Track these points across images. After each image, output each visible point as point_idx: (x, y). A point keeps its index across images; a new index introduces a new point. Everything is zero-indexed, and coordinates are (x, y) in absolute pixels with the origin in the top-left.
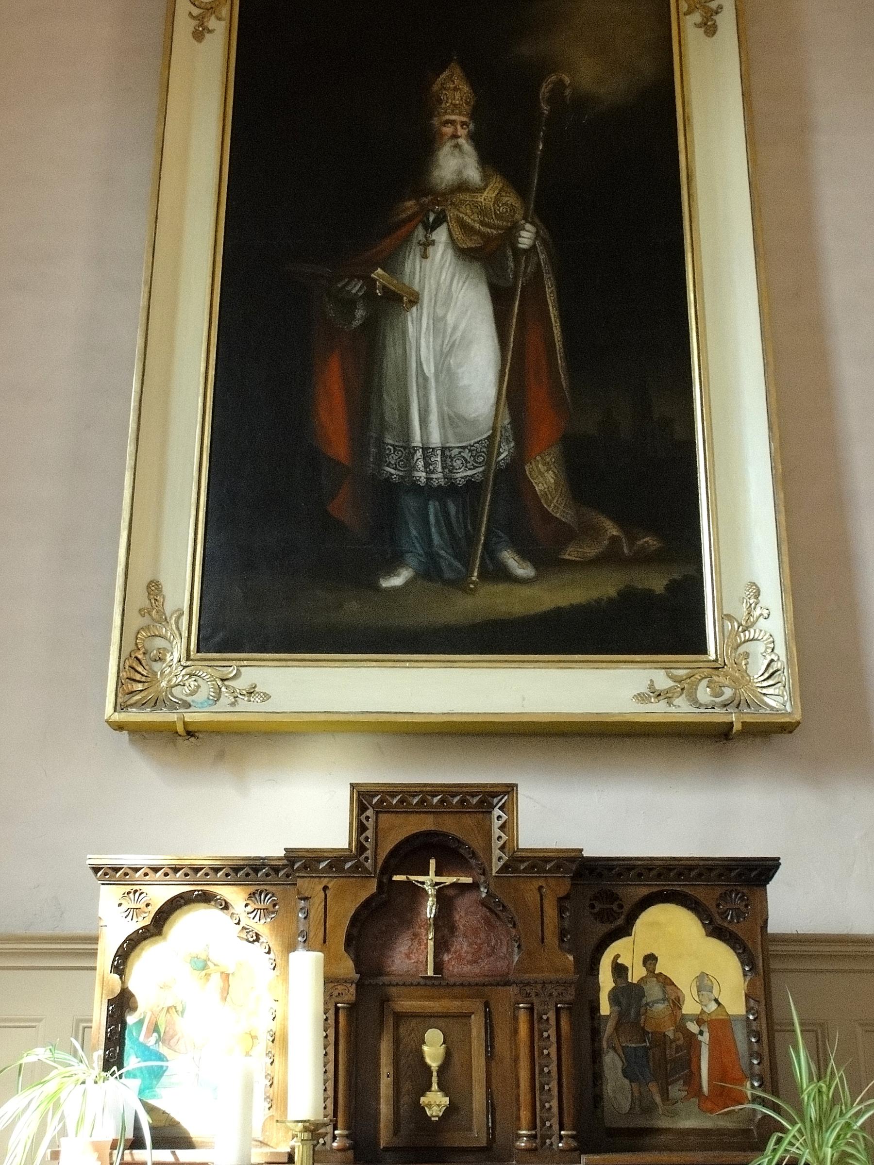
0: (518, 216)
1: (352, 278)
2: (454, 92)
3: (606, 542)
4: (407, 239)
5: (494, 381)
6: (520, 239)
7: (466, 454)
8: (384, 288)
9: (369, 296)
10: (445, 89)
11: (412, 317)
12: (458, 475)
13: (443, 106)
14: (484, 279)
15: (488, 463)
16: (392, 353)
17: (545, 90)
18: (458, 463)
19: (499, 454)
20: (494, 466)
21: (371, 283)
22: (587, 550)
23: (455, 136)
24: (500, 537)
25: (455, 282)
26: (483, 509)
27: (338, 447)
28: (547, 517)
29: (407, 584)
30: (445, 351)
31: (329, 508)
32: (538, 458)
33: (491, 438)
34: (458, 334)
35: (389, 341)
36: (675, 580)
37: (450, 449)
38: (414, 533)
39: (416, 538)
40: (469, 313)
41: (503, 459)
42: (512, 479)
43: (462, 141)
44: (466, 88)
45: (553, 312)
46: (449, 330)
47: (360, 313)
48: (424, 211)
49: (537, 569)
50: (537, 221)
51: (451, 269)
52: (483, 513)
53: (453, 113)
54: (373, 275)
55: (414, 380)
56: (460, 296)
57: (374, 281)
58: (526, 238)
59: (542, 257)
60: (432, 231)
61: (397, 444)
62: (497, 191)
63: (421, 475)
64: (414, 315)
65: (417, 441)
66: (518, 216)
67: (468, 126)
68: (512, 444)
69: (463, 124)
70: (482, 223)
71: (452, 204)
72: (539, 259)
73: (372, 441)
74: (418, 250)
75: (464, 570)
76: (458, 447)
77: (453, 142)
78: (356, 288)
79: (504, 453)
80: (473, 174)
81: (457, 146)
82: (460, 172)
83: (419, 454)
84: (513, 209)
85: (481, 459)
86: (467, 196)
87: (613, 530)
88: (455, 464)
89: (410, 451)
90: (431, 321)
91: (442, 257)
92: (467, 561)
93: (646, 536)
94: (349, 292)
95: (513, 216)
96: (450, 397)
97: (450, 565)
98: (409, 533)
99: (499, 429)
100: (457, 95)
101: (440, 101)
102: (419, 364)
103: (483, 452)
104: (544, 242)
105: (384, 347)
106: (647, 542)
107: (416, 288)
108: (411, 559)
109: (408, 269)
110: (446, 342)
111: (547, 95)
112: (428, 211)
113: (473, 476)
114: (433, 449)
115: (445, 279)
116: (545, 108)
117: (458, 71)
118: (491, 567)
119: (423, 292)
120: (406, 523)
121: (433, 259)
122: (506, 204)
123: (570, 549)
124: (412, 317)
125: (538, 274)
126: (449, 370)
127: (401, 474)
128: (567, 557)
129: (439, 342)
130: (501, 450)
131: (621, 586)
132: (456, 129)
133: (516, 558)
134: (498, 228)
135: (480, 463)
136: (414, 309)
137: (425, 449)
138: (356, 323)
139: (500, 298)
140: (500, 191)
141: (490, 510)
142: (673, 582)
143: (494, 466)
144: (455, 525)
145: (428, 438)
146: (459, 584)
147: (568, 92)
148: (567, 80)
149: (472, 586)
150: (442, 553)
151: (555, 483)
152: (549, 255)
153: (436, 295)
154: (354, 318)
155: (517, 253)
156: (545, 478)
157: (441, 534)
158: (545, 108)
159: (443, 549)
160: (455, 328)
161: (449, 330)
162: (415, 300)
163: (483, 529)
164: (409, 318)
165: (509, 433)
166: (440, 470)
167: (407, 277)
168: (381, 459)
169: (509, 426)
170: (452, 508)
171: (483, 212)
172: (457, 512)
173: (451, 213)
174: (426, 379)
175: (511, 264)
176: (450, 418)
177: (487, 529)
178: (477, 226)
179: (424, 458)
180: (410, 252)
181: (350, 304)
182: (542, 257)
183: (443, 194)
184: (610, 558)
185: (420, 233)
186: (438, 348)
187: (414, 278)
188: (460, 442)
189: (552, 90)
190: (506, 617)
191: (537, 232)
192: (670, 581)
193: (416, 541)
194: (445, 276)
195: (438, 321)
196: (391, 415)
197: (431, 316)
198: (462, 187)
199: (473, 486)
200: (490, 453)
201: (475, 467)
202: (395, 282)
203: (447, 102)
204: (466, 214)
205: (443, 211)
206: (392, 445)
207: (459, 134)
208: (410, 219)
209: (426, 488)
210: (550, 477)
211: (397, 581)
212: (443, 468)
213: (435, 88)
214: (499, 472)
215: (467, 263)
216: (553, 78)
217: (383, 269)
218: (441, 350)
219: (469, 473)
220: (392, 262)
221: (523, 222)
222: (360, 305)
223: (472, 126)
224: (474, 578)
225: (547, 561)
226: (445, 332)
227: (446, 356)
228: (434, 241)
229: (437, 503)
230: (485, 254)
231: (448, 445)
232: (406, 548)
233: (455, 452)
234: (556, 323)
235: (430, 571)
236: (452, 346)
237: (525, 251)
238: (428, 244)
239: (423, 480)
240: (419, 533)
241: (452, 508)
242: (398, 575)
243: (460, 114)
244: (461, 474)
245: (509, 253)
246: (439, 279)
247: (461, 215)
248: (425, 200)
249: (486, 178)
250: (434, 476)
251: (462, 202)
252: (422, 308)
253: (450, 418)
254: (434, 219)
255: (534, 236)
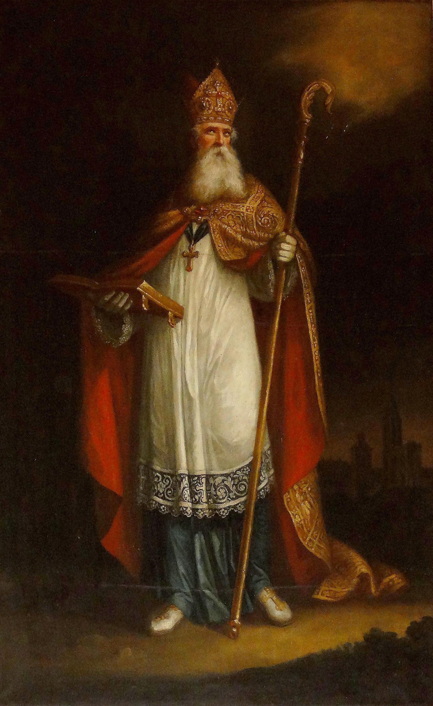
0: (279, 228)
1: (118, 291)
2: (217, 102)
3: (355, 581)
4: (171, 250)
5: (255, 402)
6: (281, 252)
7: (229, 483)
8: (150, 303)
9: (136, 311)
10: (207, 95)
11: (177, 333)
12: (221, 506)
13: (205, 113)
14: (246, 293)
15: (249, 492)
16: (157, 356)
17: (307, 98)
18: (221, 493)
19: (260, 482)
20: (254, 497)
21: (136, 296)
22: (338, 589)
23: (218, 144)
24: (260, 575)
25: (218, 295)
26: (245, 543)
27: (108, 473)
28: (303, 552)
29: (177, 627)
30: (209, 369)
31: (103, 542)
32: (296, 487)
33: (252, 465)
34: (221, 352)
35: (156, 358)
36: (416, 622)
37: (214, 476)
38: (182, 570)
39: (183, 575)
40: (232, 329)
41: (263, 488)
42: (270, 509)
43: (225, 149)
44: (228, 95)
45: (312, 330)
46: (213, 348)
47: (127, 329)
48: (187, 220)
49: (293, 609)
50: (297, 233)
51: (214, 283)
52: (244, 548)
53: (215, 120)
54: (138, 288)
55: (180, 401)
56: (223, 311)
57: (140, 294)
58: (287, 251)
59: (302, 270)
60: (195, 243)
61: (165, 471)
62: (259, 202)
63: (187, 505)
64: (179, 331)
65: (183, 469)
66: (279, 228)
67: (230, 133)
68: (272, 472)
69: (226, 131)
70: (245, 234)
71: (215, 214)
72: (299, 273)
73: (142, 467)
74: (182, 261)
75: (226, 611)
76: (222, 475)
77: (216, 150)
78: (123, 302)
79: (265, 481)
80: (235, 183)
81: (219, 154)
82: (223, 181)
83: (185, 482)
84: (274, 221)
85: (242, 488)
86: (228, 207)
87: (362, 567)
88: (218, 493)
89: (175, 478)
90: (196, 339)
91: (206, 270)
92: (228, 600)
93: (392, 574)
94: (116, 306)
95: (274, 228)
96: (213, 422)
97: (215, 606)
98: (177, 569)
99: (260, 456)
100: (220, 102)
101: (202, 108)
102: (185, 384)
103: (245, 480)
104: (304, 254)
105: (152, 367)
106: (391, 580)
107: (181, 302)
108: (179, 599)
109: (172, 282)
110: (209, 361)
111: (309, 103)
112: (192, 221)
113: (235, 507)
114: (199, 477)
115: (209, 293)
116: (307, 117)
117: (221, 78)
118: (252, 609)
119: (187, 307)
120: (174, 556)
121: (197, 273)
122: (268, 215)
123: (323, 588)
124: (177, 333)
125: (298, 288)
126: (213, 391)
127: (169, 504)
128: (320, 597)
129: (203, 359)
130: (261, 478)
131: (367, 630)
132: (219, 138)
133: (274, 598)
134: (259, 240)
135: (242, 492)
136: (179, 324)
137: (191, 477)
138: (124, 339)
139: (261, 312)
140: (262, 201)
141: (251, 544)
142: (414, 623)
143: (254, 497)
144: (218, 559)
145: (194, 465)
146: (222, 627)
147: (329, 101)
148: (329, 89)
149: (235, 630)
150: (207, 592)
151: (311, 514)
152: (309, 270)
153: (200, 310)
154: (121, 333)
155: (276, 263)
156: (302, 509)
157: (206, 571)
158: (307, 117)
159: (208, 589)
160: (218, 346)
161: (213, 348)
162: (180, 315)
163: (245, 566)
164: (174, 334)
165: (269, 460)
166: (204, 499)
167: (172, 291)
168: (150, 488)
169: (269, 452)
170: (216, 542)
171: (245, 223)
172: (221, 546)
173: (214, 224)
174: (190, 399)
175: (272, 277)
176: (214, 442)
177: (250, 564)
178: (239, 237)
179: (190, 487)
180: (174, 265)
181: (115, 319)
182: (302, 270)
183: (205, 204)
184: (359, 598)
185: (183, 244)
186: (202, 368)
187: (179, 292)
188: (224, 469)
189: (314, 98)
190: (264, 665)
191: (298, 245)
192: (411, 623)
193: (183, 579)
194: (208, 290)
195: (201, 338)
196: (159, 440)
197: (195, 334)
198: (225, 197)
199: (236, 518)
200: (250, 482)
201: (237, 497)
202: (160, 296)
203: (209, 109)
204: (229, 225)
205: (206, 221)
206: (161, 473)
207: (222, 141)
208: (177, 227)
209: (192, 519)
210: (306, 508)
211: (165, 624)
212: (208, 498)
213: (198, 94)
214: (260, 502)
215: (230, 276)
216: (315, 86)
217: (150, 283)
218: (205, 370)
219: (232, 503)
220: (157, 276)
221: (284, 234)
222: (127, 319)
223: (234, 134)
224: (236, 621)
225: (302, 603)
226: (208, 349)
227: (210, 376)
228: (197, 252)
229: (202, 537)
230: (247, 267)
231: (212, 472)
232: (175, 587)
233: (219, 480)
234: (314, 340)
235: (197, 614)
236: (216, 364)
237: (286, 265)
238: (191, 256)
239: (189, 511)
240: (187, 570)
241: (216, 542)
242: (167, 617)
243: (223, 121)
244: (225, 505)
245: (270, 266)
246: (203, 293)
247: (225, 226)
248: (188, 210)
249: (248, 187)
250: (199, 507)
251: (224, 213)
252: (186, 324)
253: (214, 442)
254: (197, 231)
255: (294, 249)
